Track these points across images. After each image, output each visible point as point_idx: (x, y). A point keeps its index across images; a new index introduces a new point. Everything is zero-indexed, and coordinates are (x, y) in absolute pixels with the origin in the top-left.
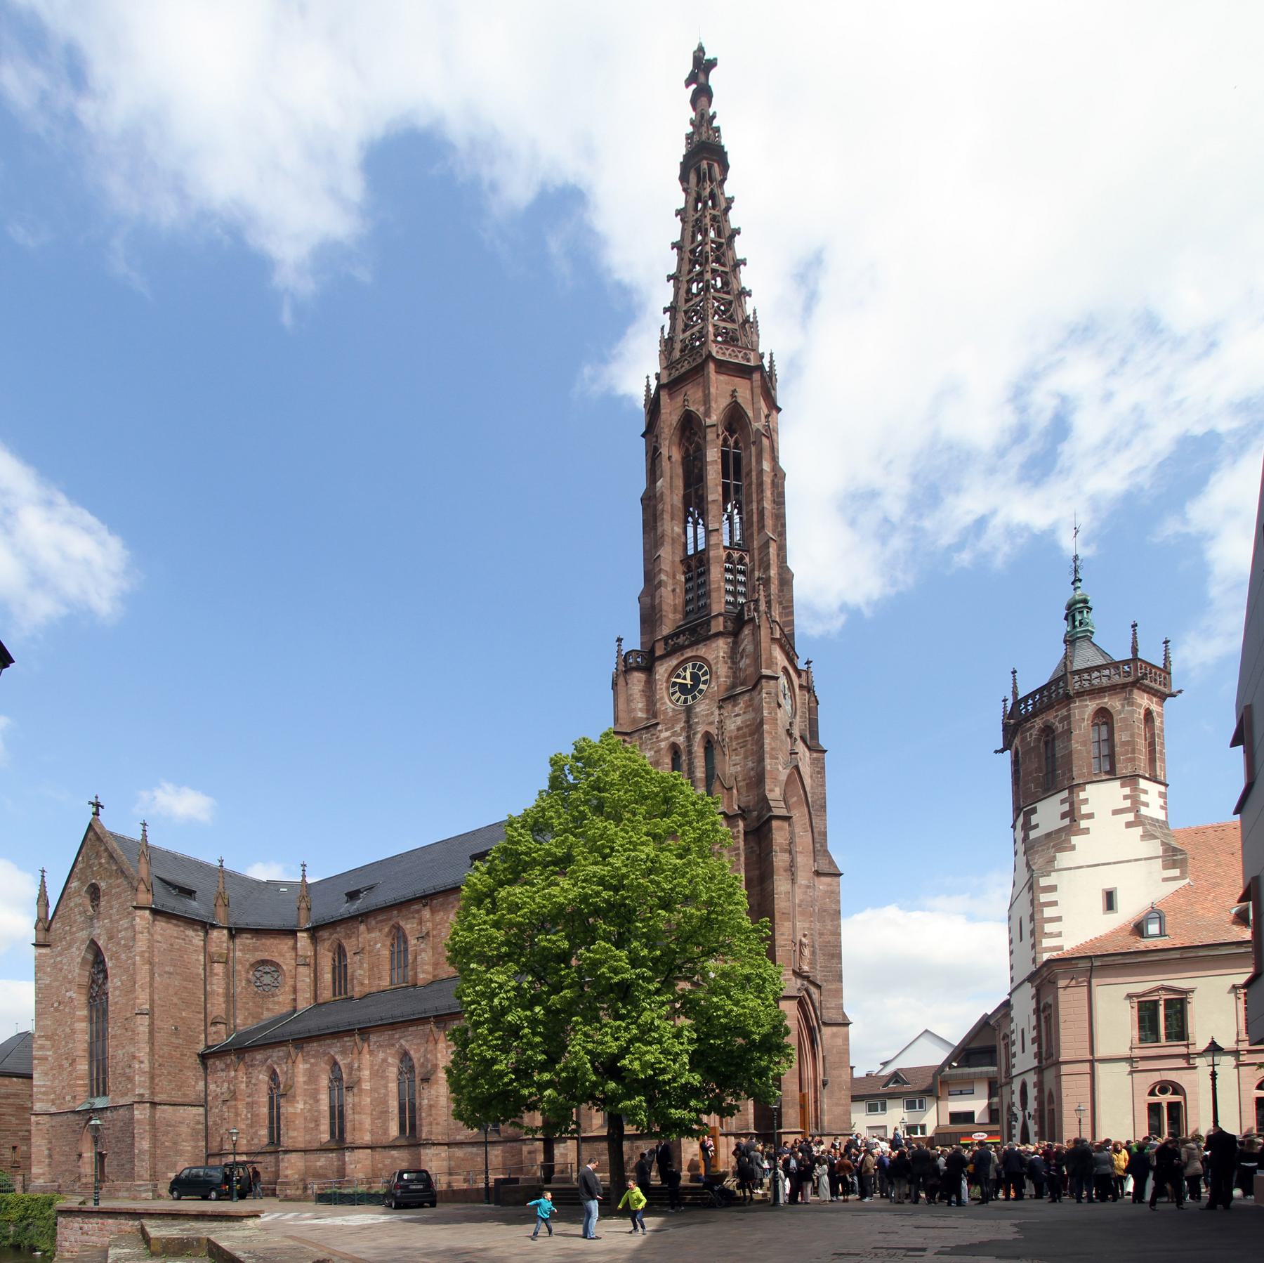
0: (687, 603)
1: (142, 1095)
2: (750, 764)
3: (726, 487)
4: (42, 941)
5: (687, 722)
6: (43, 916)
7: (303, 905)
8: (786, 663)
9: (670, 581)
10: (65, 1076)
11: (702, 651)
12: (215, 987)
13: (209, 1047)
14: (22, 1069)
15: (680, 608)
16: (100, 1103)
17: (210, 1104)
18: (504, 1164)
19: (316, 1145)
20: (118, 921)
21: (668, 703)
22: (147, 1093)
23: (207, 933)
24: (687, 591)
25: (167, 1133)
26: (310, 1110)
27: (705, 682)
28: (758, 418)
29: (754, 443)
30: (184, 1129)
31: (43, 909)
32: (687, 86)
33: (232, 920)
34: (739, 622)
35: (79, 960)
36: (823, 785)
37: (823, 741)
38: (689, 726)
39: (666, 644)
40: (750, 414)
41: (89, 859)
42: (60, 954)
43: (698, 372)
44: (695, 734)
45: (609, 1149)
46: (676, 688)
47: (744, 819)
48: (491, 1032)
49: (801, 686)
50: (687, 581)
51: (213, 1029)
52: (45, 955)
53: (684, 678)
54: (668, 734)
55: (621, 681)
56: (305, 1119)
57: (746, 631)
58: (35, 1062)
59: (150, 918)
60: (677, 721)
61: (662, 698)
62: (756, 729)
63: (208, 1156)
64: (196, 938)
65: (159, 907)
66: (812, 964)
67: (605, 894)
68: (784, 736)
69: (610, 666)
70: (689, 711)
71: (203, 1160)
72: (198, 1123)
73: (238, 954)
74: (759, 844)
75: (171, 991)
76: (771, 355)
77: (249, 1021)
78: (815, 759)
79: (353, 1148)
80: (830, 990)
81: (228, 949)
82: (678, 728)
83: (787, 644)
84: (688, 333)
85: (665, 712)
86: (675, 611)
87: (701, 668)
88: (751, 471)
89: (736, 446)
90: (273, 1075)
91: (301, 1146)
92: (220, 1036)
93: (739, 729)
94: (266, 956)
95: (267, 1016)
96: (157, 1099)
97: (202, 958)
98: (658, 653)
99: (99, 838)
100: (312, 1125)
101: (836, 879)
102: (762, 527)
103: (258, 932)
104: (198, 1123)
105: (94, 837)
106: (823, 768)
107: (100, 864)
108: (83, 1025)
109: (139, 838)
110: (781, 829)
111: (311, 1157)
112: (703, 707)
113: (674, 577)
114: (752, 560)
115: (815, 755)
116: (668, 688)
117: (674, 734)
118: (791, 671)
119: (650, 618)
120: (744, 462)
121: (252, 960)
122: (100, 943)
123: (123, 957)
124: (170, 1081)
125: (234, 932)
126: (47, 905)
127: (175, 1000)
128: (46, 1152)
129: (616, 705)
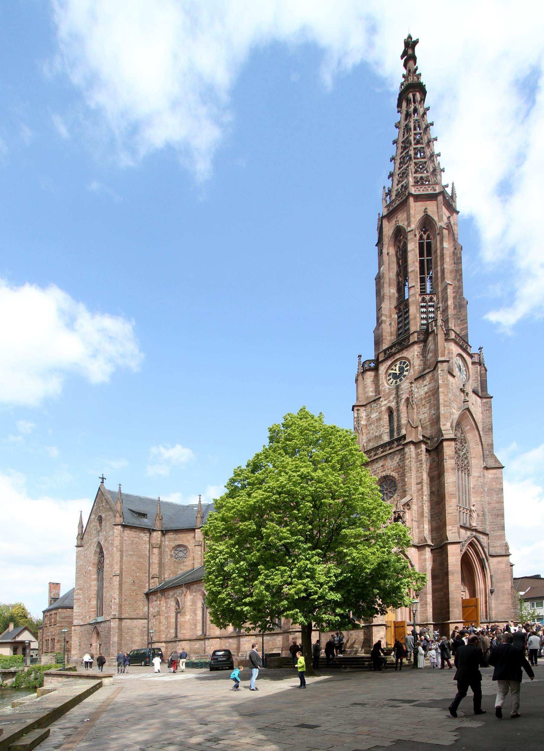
0: (399, 329)
1: (115, 615)
2: (433, 412)
3: (421, 263)
4: (79, 544)
5: (397, 394)
6: (81, 533)
7: (199, 516)
8: (461, 352)
9: (388, 319)
10: (87, 607)
11: (405, 354)
12: (154, 560)
13: (150, 590)
14: (516, 581)
15: (395, 333)
16: (100, 619)
17: (150, 618)
18: (283, 645)
19: (195, 637)
20: (109, 532)
21: (386, 385)
22: (117, 614)
23: (150, 534)
24: (399, 323)
25: (127, 633)
26: (193, 619)
27: (407, 371)
28: (441, 219)
29: (438, 234)
30: (136, 631)
31: (81, 529)
32: (402, 58)
33: (164, 526)
34: (426, 334)
35: (94, 552)
36: (490, 417)
37: (490, 392)
38: (398, 396)
39: (385, 354)
40: (436, 219)
41: (99, 504)
42: (87, 550)
43: (404, 204)
44: (401, 400)
45: (302, 636)
46: (391, 377)
47: (426, 443)
48: (217, 577)
49: (473, 363)
50: (399, 317)
51: (152, 581)
52: (81, 551)
53: (395, 370)
54: (386, 402)
55: (360, 378)
56: (190, 624)
57: (430, 338)
58: (75, 601)
59: (122, 529)
60: (391, 394)
61: (383, 383)
62: (435, 393)
63: (149, 644)
64: (145, 537)
65: (126, 524)
66: (483, 522)
67: (274, 497)
68: (458, 392)
69: (355, 369)
70: (398, 388)
71: (146, 646)
72: (144, 627)
73: (167, 543)
74: (438, 455)
75: (132, 563)
76: (453, 184)
77: (171, 576)
78: (484, 403)
79: (209, 638)
80: (496, 536)
81: (161, 541)
82: (391, 398)
83: (462, 342)
84: (400, 185)
85: (384, 391)
86: (391, 335)
87: (405, 363)
88: (436, 250)
89: (428, 238)
90: (177, 603)
91: (188, 637)
92: (155, 584)
93: (426, 393)
94: (180, 543)
95: (180, 572)
96: (123, 617)
97: (148, 546)
98: (380, 360)
99: (102, 494)
100: (193, 627)
101: (500, 470)
102: (443, 278)
103: (177, 531)
104: (144, 627)
105: (101, 494)
106: (491, 407)
107: (103, 506)
108: (95, 583)
109: (117, 490)
110: (450, 446)
111: (193, 643)
112: (405, 384)
113: (391, 317)
114: (438, 298)
115: (485, 400)
116: (386, 378)
117: (389, 402)
118: (465, 355)
119: (378, 342)
120: (433, 246)
121: (173, 545)
122: (102, 543)
123: (110, 549)
124: (130, 607)
125: (164, 532)
126: (83, 527)
127: (134, 568)
128: (78, 644)
129: (357, 391)
